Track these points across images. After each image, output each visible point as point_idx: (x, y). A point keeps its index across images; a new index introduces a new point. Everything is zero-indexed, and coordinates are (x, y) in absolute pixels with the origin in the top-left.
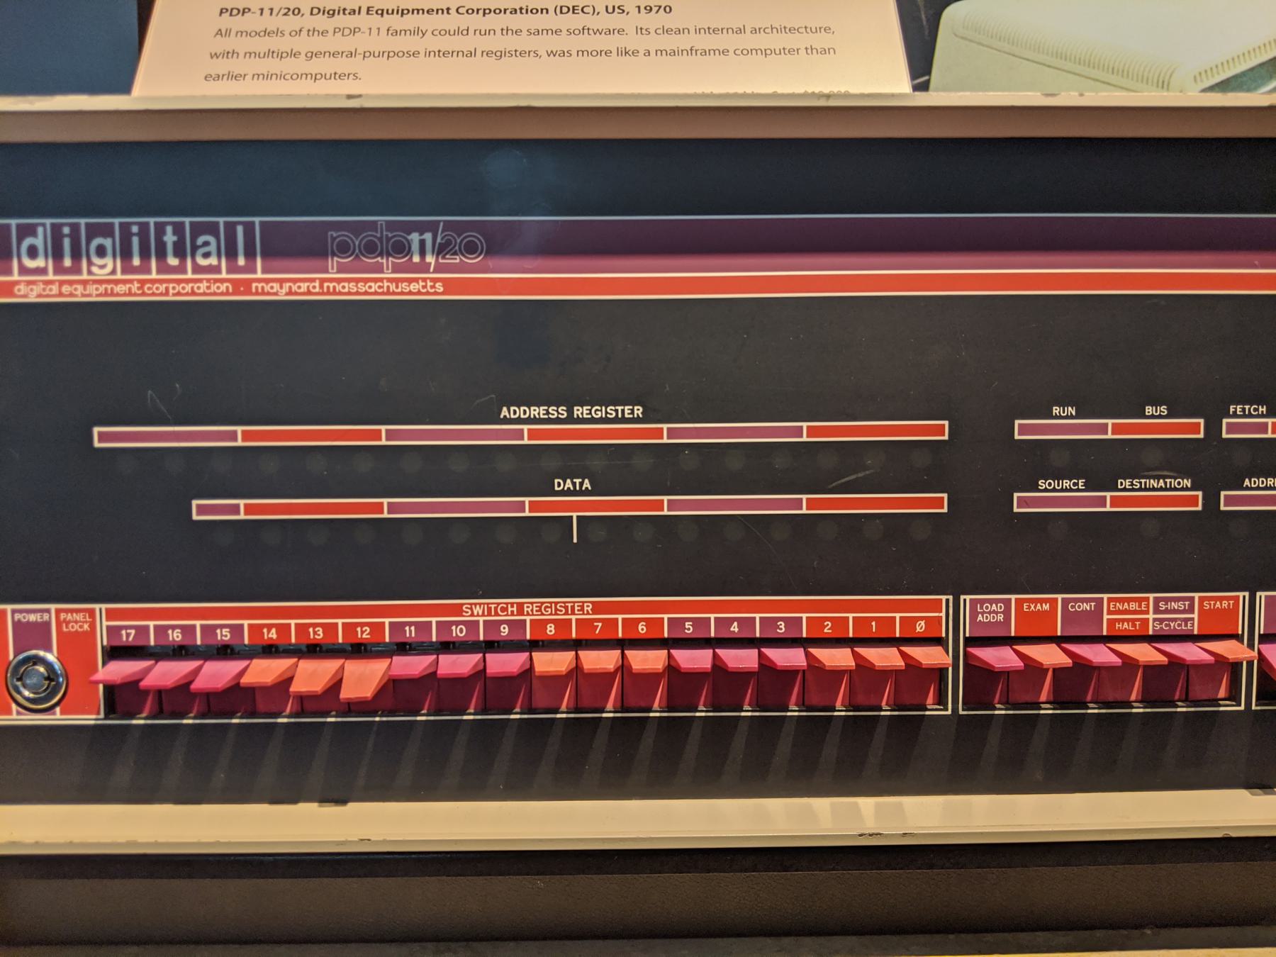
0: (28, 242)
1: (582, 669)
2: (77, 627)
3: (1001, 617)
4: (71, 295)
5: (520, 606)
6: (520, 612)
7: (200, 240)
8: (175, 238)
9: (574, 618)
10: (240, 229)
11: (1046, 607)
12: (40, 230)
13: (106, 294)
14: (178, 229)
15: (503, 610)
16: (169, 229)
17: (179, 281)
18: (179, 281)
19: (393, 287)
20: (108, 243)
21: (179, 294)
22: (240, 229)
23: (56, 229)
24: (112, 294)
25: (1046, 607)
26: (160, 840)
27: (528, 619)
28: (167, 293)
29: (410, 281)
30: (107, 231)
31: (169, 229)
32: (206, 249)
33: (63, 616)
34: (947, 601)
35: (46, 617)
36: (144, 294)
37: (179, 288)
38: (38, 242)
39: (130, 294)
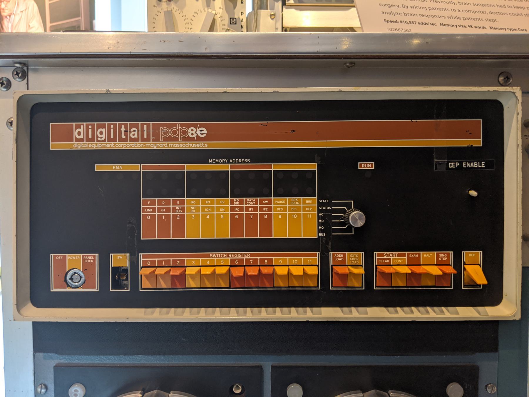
0: (78, 130)
1: (247, 274)
2: (89, 261)
3: (342, 259)
4: (92, 147)
5: (228, 255)
6: (228, 256)
7: (132, 130)
8: (125, 129)
9: (244, 258)
10: (145, 126)
11: (417, 256)
12: (82, 126)
13: (103, 147)
14: (126, 126)
15: (223, 256)
16: (123, 126)
17: (127, 144)
18: (127, 144)
19: (191, 145)
20: (103, 130)
21: (126, 147)
22: (145, 126)
23: (87, 126)
24: (105, 147)
25: (417, 256)
26: (15, 234)
27: (391, 258)
28: (123, 147)
29: (197, 143)
30: (104, 127)
31: (123, 126)
32: (134, 133)
33: (84, 257)
34: (144, 257)
35: (79, 258)
36: (115, 147)
37: (126, 145)
38: (81, 130)
39: (111, 147)
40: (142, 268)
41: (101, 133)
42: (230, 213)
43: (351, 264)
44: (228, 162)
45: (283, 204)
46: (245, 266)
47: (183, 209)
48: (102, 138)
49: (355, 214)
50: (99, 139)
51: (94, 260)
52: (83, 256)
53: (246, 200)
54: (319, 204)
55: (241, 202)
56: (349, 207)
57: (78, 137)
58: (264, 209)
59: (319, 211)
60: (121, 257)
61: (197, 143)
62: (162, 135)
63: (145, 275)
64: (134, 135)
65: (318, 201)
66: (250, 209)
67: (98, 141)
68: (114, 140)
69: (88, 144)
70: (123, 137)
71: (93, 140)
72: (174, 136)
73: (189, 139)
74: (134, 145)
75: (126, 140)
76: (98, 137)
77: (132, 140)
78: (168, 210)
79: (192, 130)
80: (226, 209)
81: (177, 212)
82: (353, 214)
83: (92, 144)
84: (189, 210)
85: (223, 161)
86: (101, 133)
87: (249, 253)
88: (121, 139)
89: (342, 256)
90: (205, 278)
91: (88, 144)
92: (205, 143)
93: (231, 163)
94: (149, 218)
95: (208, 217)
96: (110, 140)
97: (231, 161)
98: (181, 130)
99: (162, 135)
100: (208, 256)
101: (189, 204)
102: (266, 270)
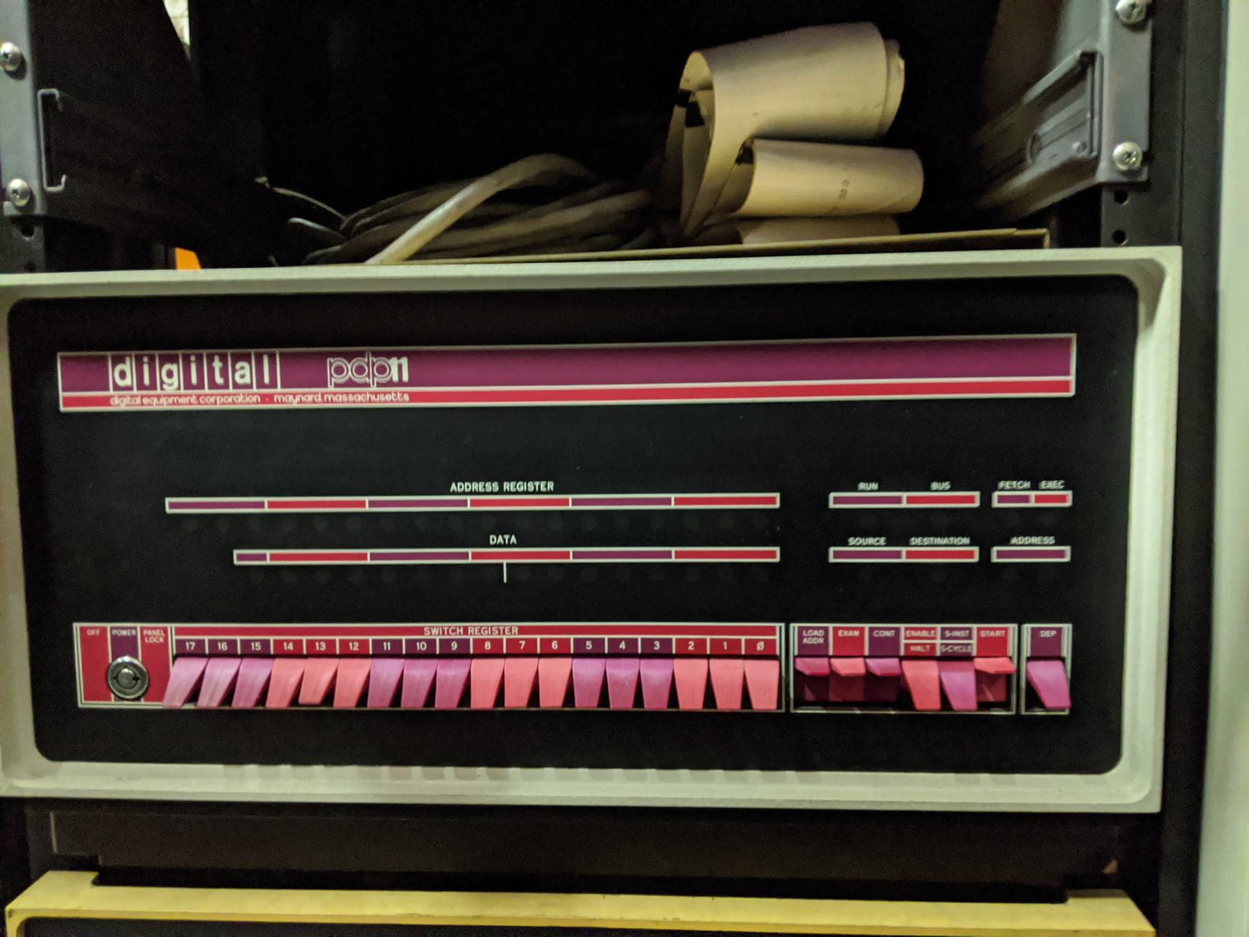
0: (119, 367)
3: (821, 641)
20: (174, 368)
25: (857, 633)
30: (174, 360)
33: (145, 632)
37: (223, 400)
39: (190, 403)
40: (175, 658)
41: (170, 374)
46: (709, 657)
48: (171, 385)
51: (826, 637)
57: (121, 383)
61: (385, 393)
64: (242, 376)
69: (142, 397)
72: (359, 379)
74: (240, 399)
76: (162, 382)
79: (242, 376)
83: (149, 396)
86: (170, 374)
87: (515, 625)
89: (821, 633)
91: (142, 397)
92: (403, 393)
100: (420, 631)
102: (881, 665)
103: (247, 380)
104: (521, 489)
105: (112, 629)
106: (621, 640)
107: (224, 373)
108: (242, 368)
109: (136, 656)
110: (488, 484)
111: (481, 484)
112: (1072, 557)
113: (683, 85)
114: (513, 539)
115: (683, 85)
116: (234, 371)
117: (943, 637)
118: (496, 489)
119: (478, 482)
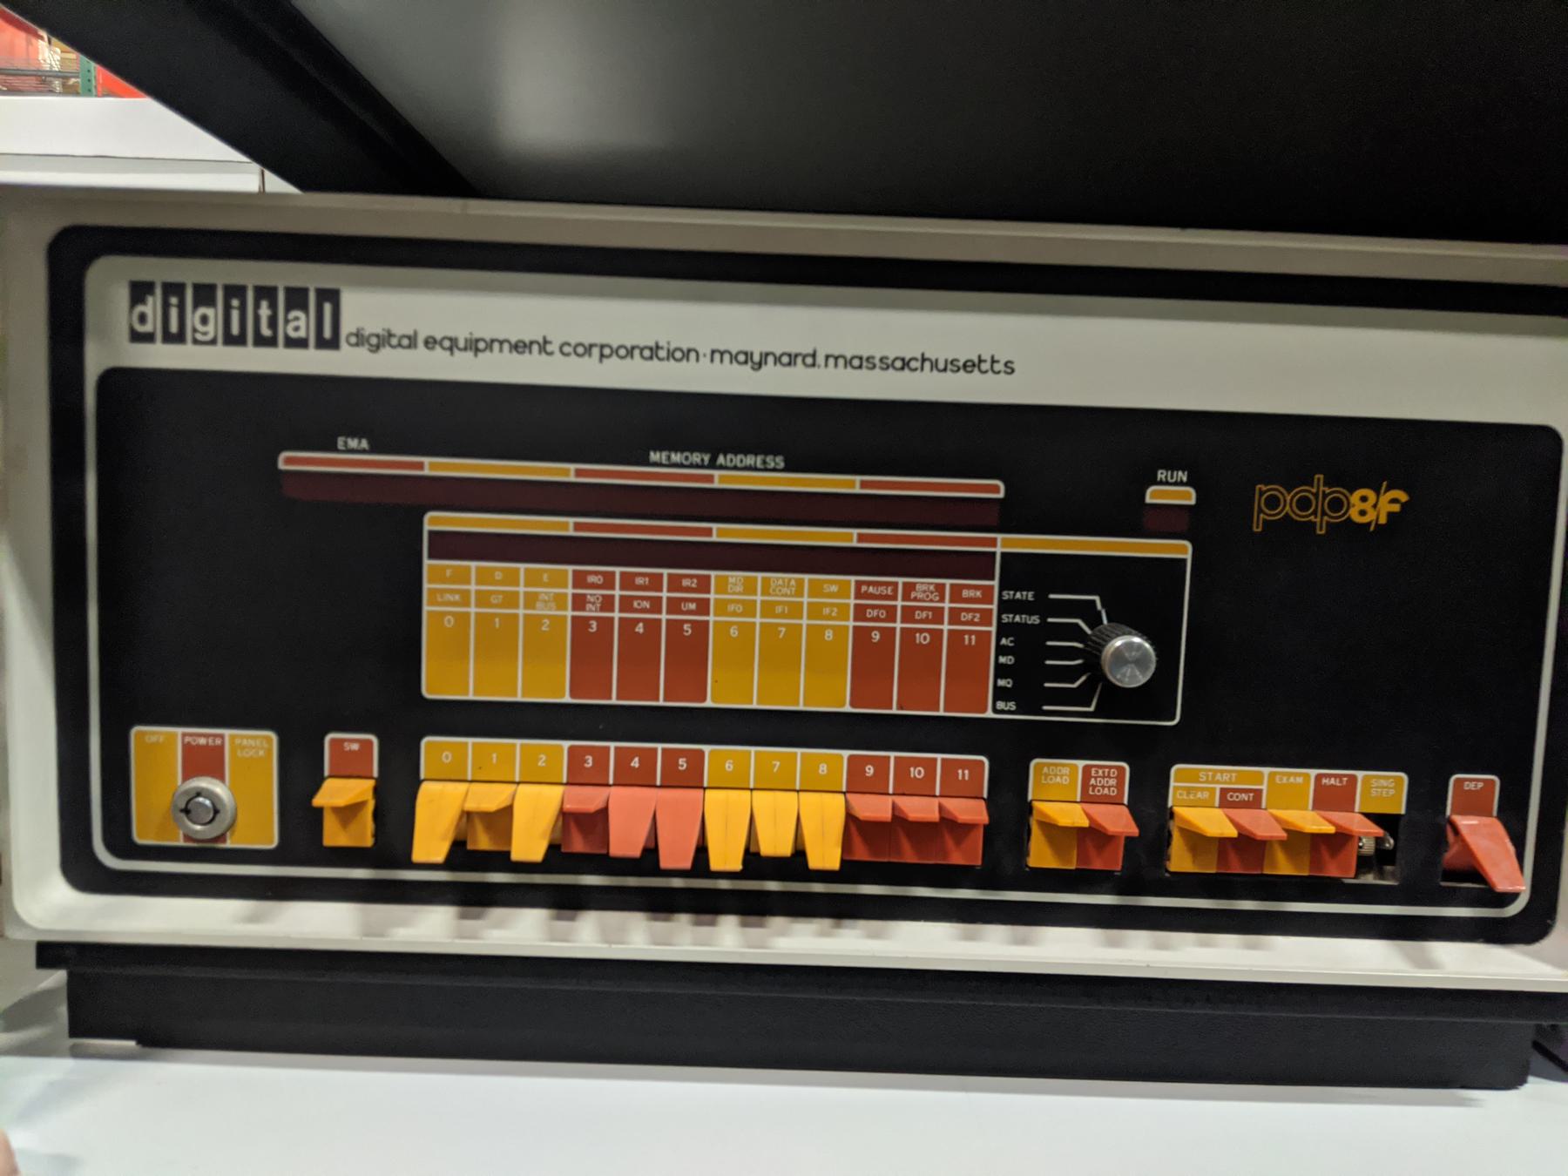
20: (210, 312)
41: (204, 320)
42: (851, 624)
43: (1070, 796)
44: (713, 465)
45: (887, 597)
47: (703, 607)
48: (205, 334)
49: (1129, 645)
50: (199, 337)
52: (184, 735)
53: (766, 581)
54: (1004, 606)
55: (750, 588)
56: (1094, 621)
58: (731, 608)
59: (1003, 630)
60: (355, 747)
62: (1260, 511)
63: (337, 810)
64: (297, 329)
65: (1000, 595)
66: (779, 609)
67: (196, 342)
68: (240, 340)
70: (266, 331)
71: (179, 338)
73: (257, 306)
75: (271, 342)
77: (292, 343)
78: (511, 600)
80: (842, 612)
81: (591, 612)
82: (1118, 643)
84: (559, 601)
85: (696, 458)
86: (204, 320)
88: (261, 341)
90: (572, 824)
92: (287, 321)
93: (721, 467)
94: (449, 622)
95: (640, 628)
96: (230, 340)
97: (721, 460)
98: (1315, 513)
99: (1260, 511)
101: (722, 589)
103: (302, 334)
104: (772, 465)
105: (184, 735)
106: (638, 621)
107: (273, 323)
108: (297, 319)
109: (221, 777)
110: (769, 459)
111: (664, 454)
112: (281, 472)
113: (319, 800)
114: (364, 444)
115: (319, 800)
116: (287, 321)
117: (858, 595)
118: (759, 465)
119: (661, 451)
